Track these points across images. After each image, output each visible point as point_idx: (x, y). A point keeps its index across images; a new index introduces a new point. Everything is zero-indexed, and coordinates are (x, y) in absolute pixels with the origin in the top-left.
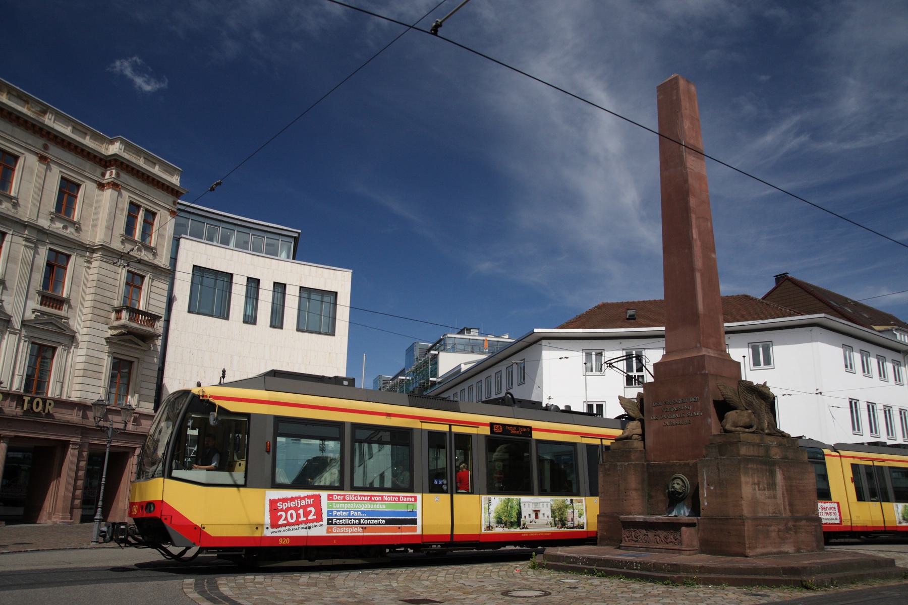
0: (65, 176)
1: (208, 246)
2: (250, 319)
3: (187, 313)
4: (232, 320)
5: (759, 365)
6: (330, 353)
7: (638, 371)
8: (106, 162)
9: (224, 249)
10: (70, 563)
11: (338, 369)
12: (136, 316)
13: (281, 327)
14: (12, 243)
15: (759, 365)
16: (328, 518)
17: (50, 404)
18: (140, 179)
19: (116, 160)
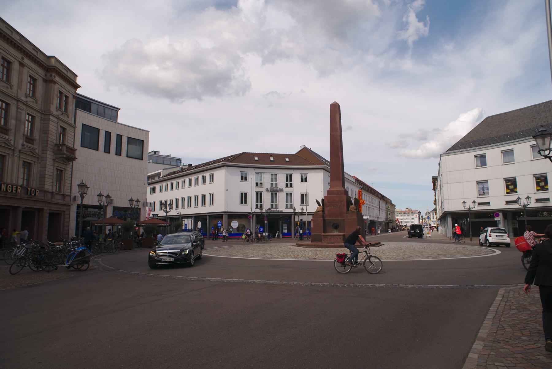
0: (4, 56)
1: (89, 114)
2: (107, 150)
3: (115, 155)
4: (100, 151)
5: (243, 180)
6: (141, 168)
7: (275, 202)
8: (47, 69)
9: (93, 116)
10: (401, 219)
11: (144, 175)
12: (533, 288)
13: (120, 155)
14: (171, 164)
15: (243, 180)
16: (526, 221)
17: (19, 189)
18: (33, 62)
19: (54, 69)
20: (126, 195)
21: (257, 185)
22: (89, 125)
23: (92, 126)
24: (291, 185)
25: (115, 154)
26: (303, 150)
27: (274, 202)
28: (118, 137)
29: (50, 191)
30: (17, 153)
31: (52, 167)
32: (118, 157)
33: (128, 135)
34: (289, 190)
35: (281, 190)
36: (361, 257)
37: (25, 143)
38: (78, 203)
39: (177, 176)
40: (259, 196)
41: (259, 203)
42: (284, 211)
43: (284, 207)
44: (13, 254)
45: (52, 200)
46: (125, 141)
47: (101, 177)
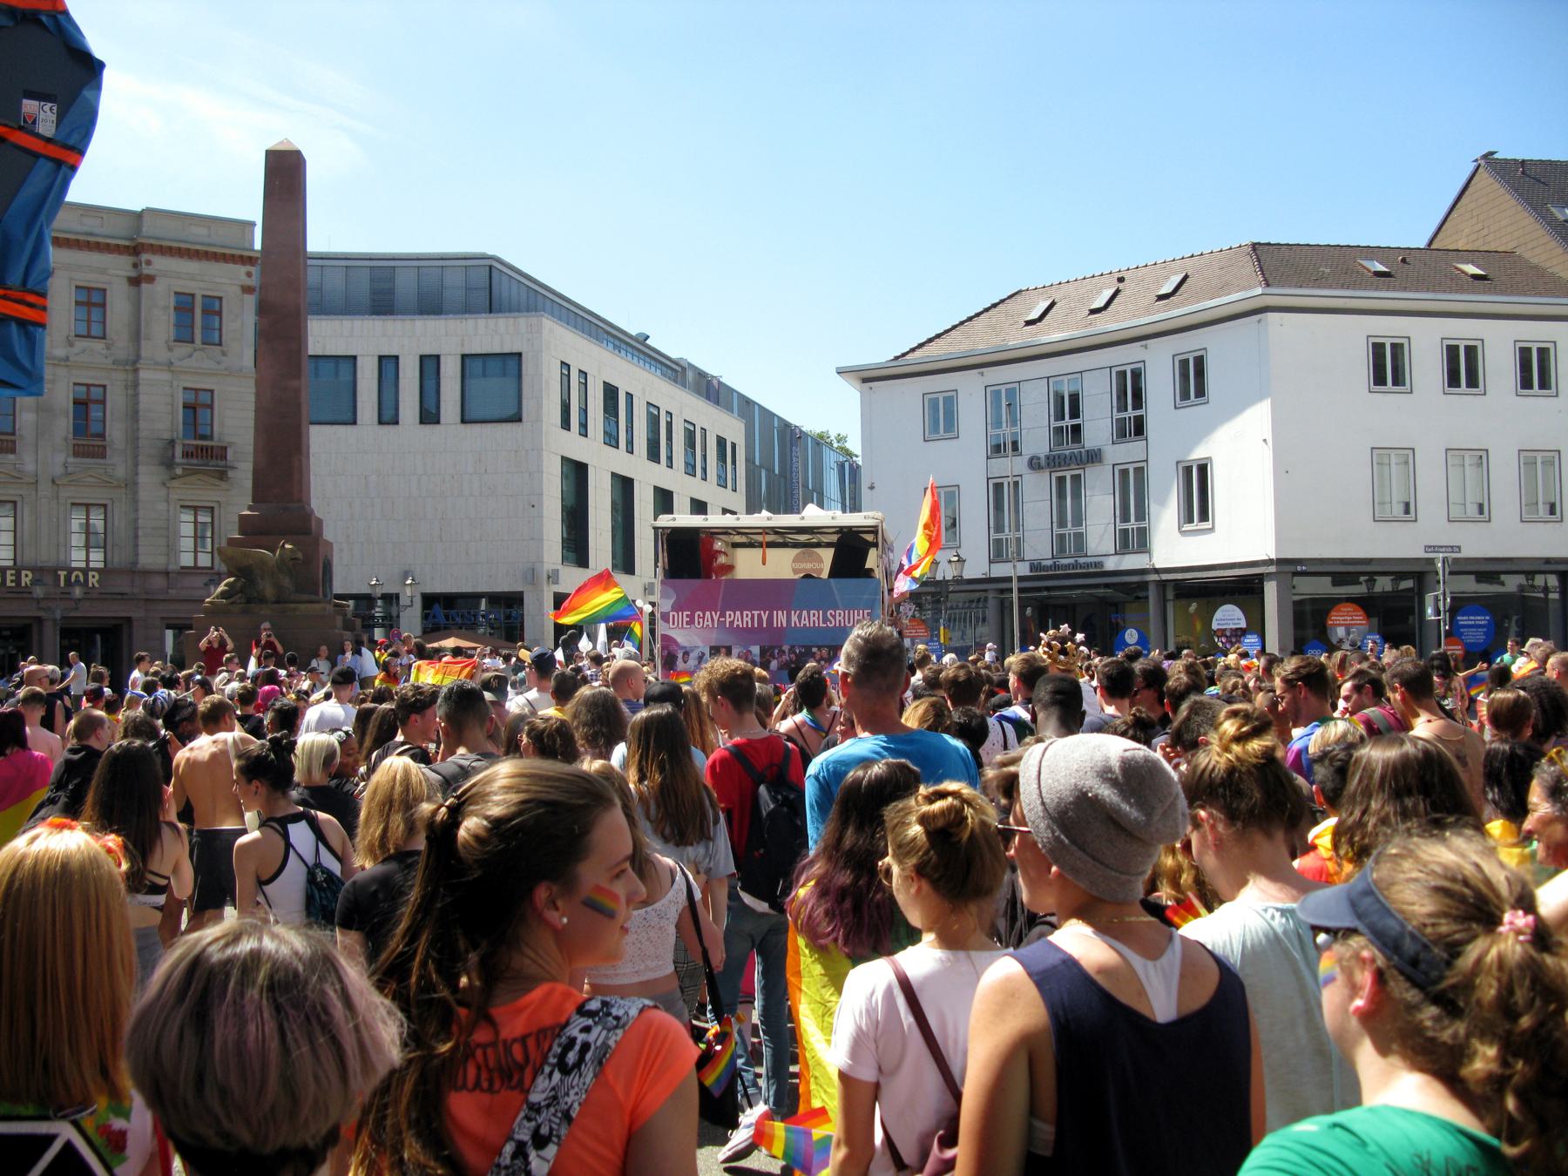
6: (516, 451)
20: (467, 553)
21: (997, 449)
22: (321, 354)
23: (328, 354)
24: (1139, 428)
25: (418, 420)
26: (329, 418)
27: (1069, 525)
28: (209, 418)
29: (162, 567)
30: (45, 489)
31: (165, 504)
32: (429, 429)
33: (462, 345)
34: (1129, 452)
35: (1034, 464)
36: (1234, 805)
37: (71, 460)
38: (428, 591)
39: (1055, 407)
40: (1001, 495)
41: (1132, 524)
42: (1111, 564)
43: (1108, 545)
44: (447, 803)
45: (167, 593)
46: (450, 371)
47: (373, 506)
